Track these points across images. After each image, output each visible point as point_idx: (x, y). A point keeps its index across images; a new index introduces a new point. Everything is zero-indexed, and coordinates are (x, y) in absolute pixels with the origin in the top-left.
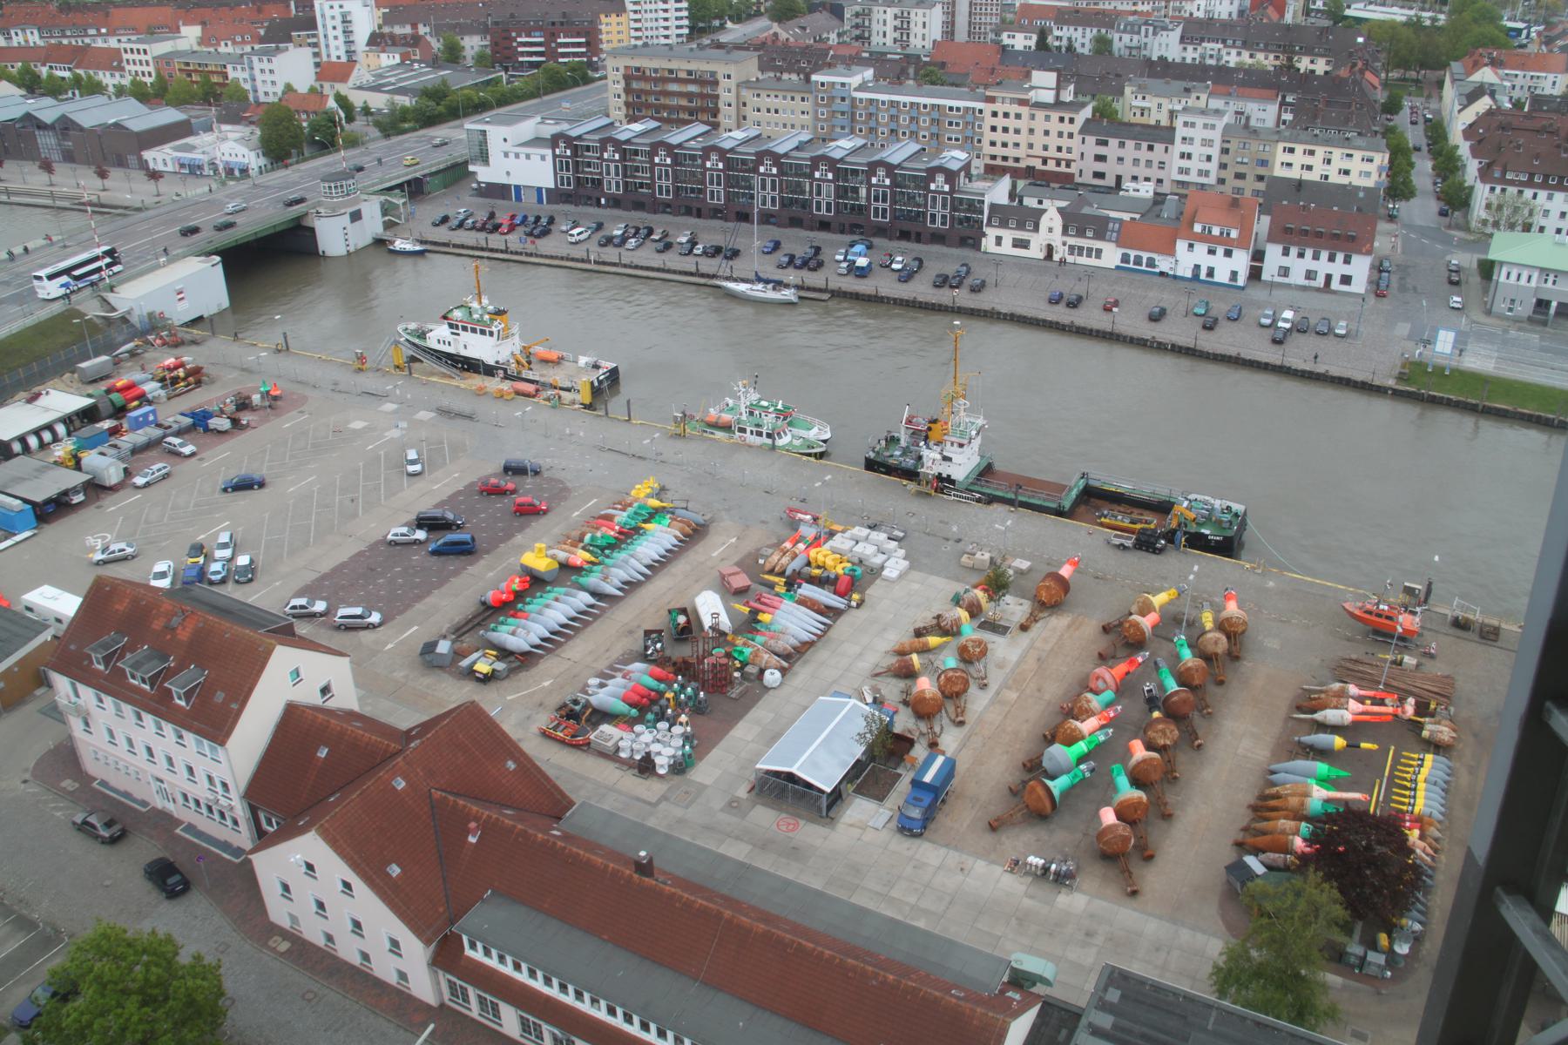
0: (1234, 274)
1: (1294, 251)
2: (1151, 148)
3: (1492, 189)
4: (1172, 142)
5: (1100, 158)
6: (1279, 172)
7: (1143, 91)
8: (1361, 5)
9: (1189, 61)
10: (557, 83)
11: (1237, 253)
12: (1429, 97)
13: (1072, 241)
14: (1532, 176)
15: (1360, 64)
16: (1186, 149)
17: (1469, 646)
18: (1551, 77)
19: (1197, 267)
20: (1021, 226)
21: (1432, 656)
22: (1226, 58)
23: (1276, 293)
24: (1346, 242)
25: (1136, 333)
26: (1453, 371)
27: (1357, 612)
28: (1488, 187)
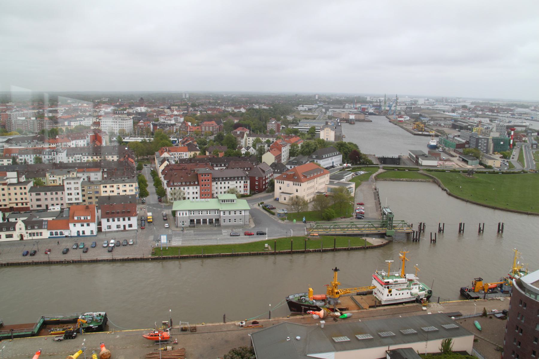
0: (92, 232)
1: (111, 220)
2: (57, 193)
3: (171, 189)
4: (64, 190)
5: (38, 200)
6: (103, 194)
7: (53, 174)
8: (128, 138)
9: (71, 162)
11: (91, 224)
12: (151, 163)
13: (30, 231)
14: (182, 183)
15: (127, 156)
16: (70, 192)
17: (189, 336)
18: (185, 153)
19: (78, 232)
20: (8, 230)
21: (177, 343)
22: (83, 159)
23: (108, 235)
24: (127, 213)
25: (58, 260)
26: (169, 248)
27: (148, 337)
28: (170, 188)
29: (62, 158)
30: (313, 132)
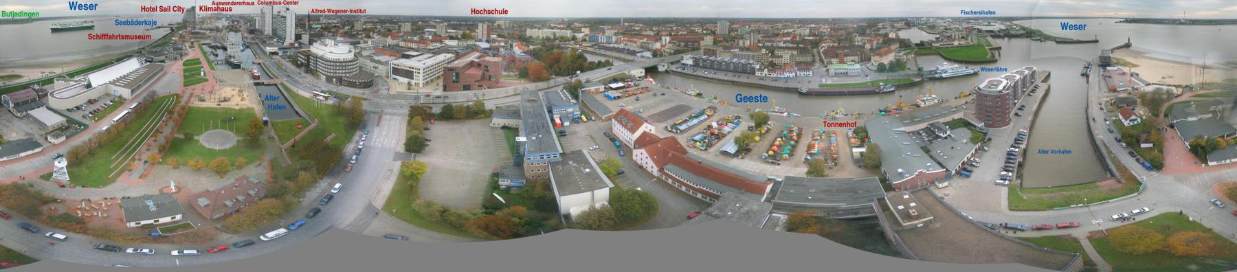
10: (694, 49)
29: (782, 44)
30: (886, 35)
